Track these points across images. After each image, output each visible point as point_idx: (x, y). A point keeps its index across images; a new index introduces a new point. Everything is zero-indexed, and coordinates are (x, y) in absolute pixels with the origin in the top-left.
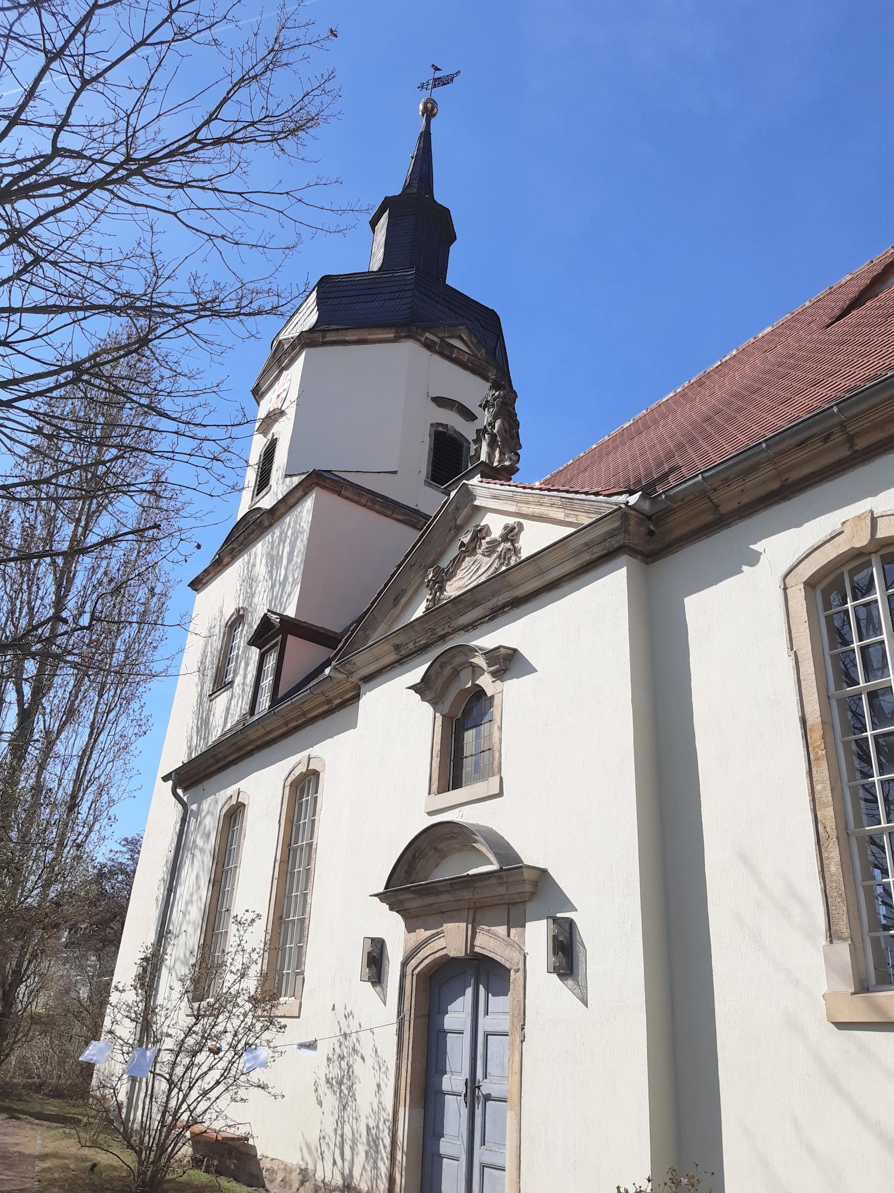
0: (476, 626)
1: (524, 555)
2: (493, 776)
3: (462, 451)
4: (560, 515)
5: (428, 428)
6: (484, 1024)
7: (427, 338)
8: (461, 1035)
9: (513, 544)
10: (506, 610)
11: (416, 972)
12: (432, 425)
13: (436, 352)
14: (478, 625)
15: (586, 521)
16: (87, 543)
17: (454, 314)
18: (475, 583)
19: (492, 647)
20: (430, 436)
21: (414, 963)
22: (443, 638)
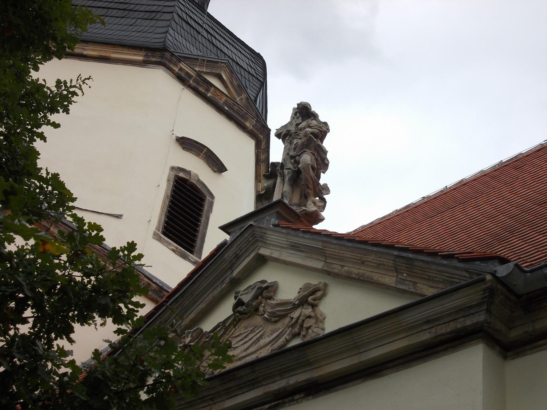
1: (330, 327)
3: (202, 206)
4: (389, 280)
5: (167, 171)
7: (181, 69)
9: (314, 310)
10: (296, 397)
12: (173, 168)
13: (190, 87)
15: (429, 292)
16: (86, 30)
17: (215, 48)
18: (253, 357)
20: (168, 180)
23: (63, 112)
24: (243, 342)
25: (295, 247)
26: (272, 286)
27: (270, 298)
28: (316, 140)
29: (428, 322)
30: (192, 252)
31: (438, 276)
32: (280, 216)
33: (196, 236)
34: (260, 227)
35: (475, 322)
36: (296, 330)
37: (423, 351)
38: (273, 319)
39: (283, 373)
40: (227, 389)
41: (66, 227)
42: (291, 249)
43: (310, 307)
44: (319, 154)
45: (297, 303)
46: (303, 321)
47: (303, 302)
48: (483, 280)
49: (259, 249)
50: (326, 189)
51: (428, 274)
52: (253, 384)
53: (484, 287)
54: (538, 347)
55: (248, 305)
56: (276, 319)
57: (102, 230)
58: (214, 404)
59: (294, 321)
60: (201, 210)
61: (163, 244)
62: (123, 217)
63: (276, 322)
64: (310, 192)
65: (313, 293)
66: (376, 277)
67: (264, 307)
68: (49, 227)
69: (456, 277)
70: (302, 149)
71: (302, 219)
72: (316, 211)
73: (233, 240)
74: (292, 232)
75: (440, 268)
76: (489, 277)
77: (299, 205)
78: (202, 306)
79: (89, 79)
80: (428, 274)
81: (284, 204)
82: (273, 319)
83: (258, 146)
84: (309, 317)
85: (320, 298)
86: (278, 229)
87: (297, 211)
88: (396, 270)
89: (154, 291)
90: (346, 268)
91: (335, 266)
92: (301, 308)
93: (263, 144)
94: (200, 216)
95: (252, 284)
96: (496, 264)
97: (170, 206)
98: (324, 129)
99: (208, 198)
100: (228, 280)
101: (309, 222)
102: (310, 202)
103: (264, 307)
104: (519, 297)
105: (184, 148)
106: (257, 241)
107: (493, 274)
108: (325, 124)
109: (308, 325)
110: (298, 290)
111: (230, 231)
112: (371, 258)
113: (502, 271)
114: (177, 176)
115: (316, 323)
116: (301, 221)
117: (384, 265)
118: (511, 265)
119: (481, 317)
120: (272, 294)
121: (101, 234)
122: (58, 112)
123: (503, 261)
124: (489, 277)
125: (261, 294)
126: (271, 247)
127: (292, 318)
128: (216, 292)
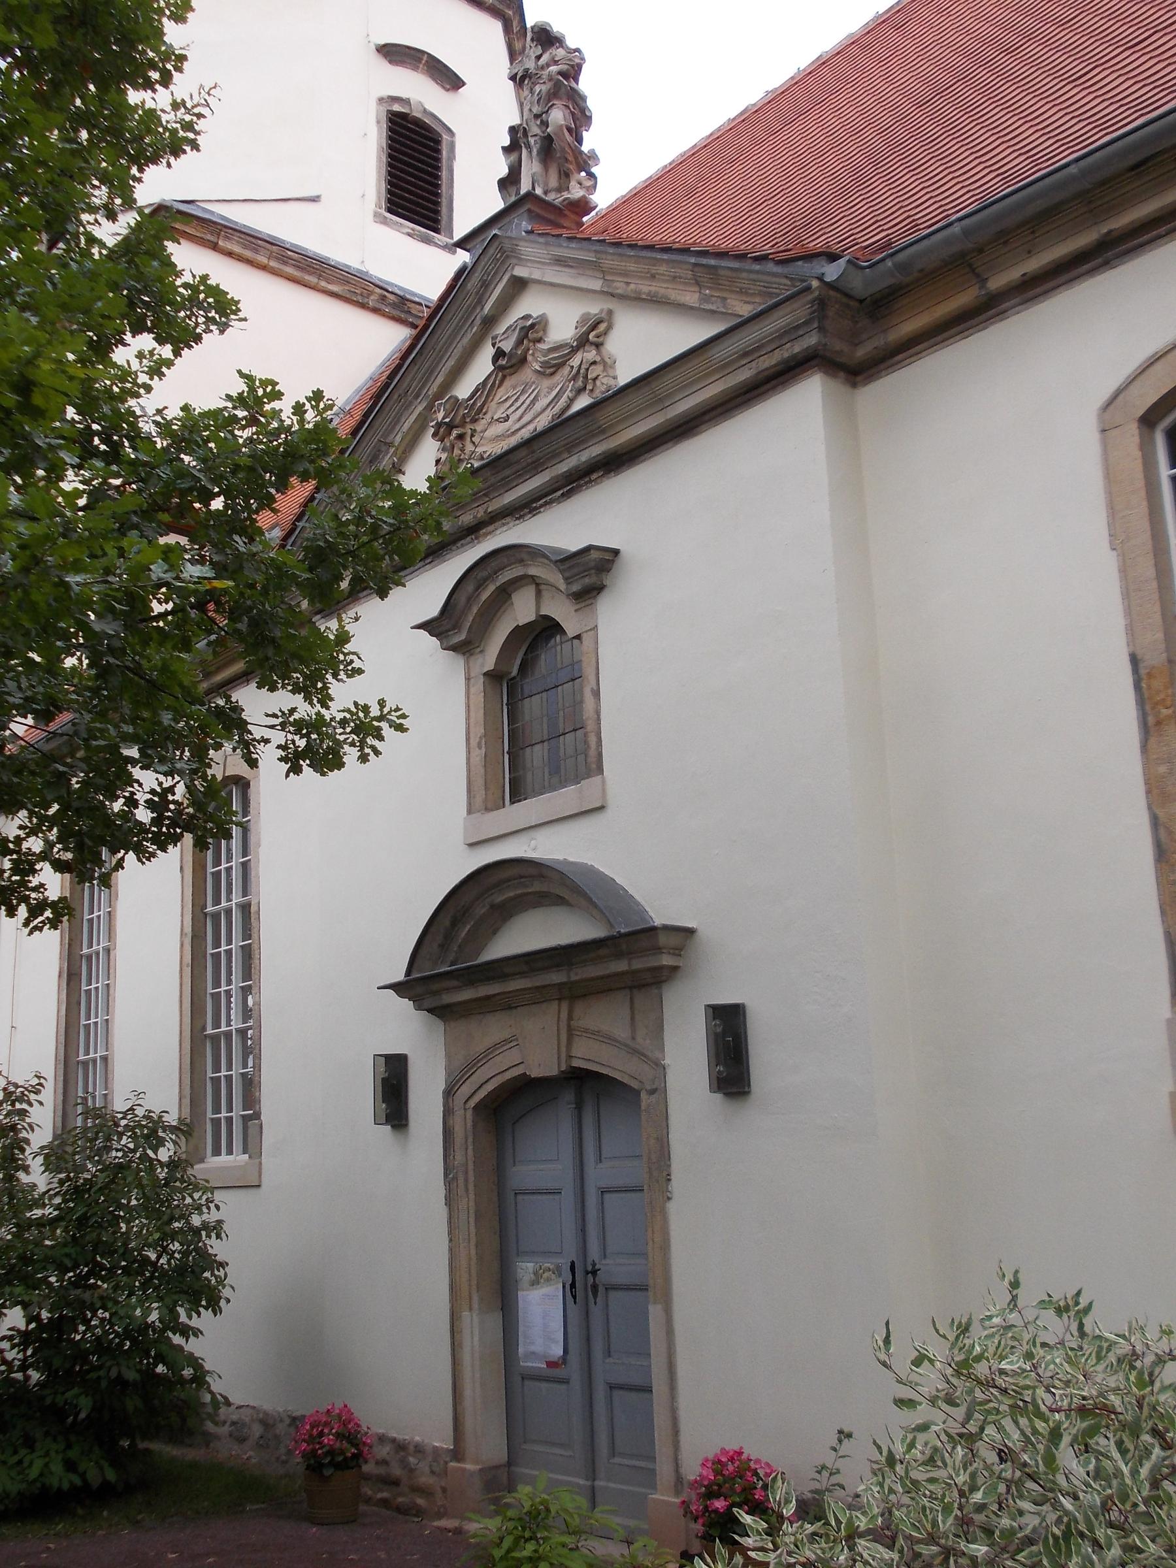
0: (536, 508)
1: (624, 376)
2: (589, 776)
3: (438, 151)
4: (690, 298)
6: (597, 1175)
8: (557, 1197)
9: (599, 353)
10: (594, 476)
11: (472, 1103)
12: (381, 100)
14: (541, 506)
15: (745, 310)
18: (526, 433)
19: (574, 547)
20: (378, 122)
21: (466, 1090)
22: (473, 531)
23: (192, 150)
24: (513, 408)
25: (560, 262)
26: (539, 323)
27: (540, 340)
28: (566, 83)
29: (746, 354)
30: (437, 231)
31: (752, 286)
32: (533, 216)
33: (437, 204)
34: (508, 237)
35: (805, 346)
36: (580, 383)
37: (745, 393)
38: (548, 371)
39: (571, 447)
40: (503, 479)
41: (243, 236)
42: (556, 264)
43: (594, 347)
44: (576, 103)
45: (575, 344)
46: (587, 370)
47: (582, 342)
48: (808, 289)
49: (513, 268)
50: (593, 157)
51: (738, 285)
52: (536, 467)
53: (810, 297)
54: (893, 365)
55: (511, 355)
56: (552, 370)
57: (278, 383)
58: (491, 500)
59: (574, 371)
60: (438, 160)
61: (391, 228)
62: (323, 198)
63: (552, 374)
64: (571, 167)
65: (594, 327)
66: (674, 295)
67: (533, 355)
68: (215, 241)
69: (774, 286)
70: (549, 101)
71: (567, 212)
72: (584, 197)
73: (474, 261)
74: (550, 239)
75: (753, 276)
76: (815, 283)
77: (559, 190)
78: (451, 362)
79: (215, 87)
80: (738, 285)
81: (537, 197)
82: (548, 371)
83: (507, 29)
84: (594, 363)
85: (605, 333)
86: (532, 237)
87: (557, 202)
88: (698, 283)
89: (394, 305)
90: (632, 286)
91: (618, 284)
92: (581, 351)
93: (515, 24)
94: (438, 168)
95: (511, 322)
96: (823, 263)
97: (390, 165)
98: (577, 61)
99: (444, 136)
100: (478, 321)
101: (577, 213)
102: (573, 183)
103: (533, 355)
104: (861, 301)
105: (390, 62)
106: (507, 257)
107: (820, 278)
108: (577, 50)
109: (594, 375)
110: (574, 324)
111: (468, 247)
112: (662, 269)
113: (832, 272)
114: (389, 112)
115: (604, 370)
116: (565, 215)
117: (680, 278)
118: (842, 262)
119: (812, 340)
120: (540, 334)
121: (277, 388)
122: (184, 152)
123: (833, 257)
124: (815, 283)
125: (526, 336)
126: (529, 264)
127: (572, 367)
128: (466, 340)
